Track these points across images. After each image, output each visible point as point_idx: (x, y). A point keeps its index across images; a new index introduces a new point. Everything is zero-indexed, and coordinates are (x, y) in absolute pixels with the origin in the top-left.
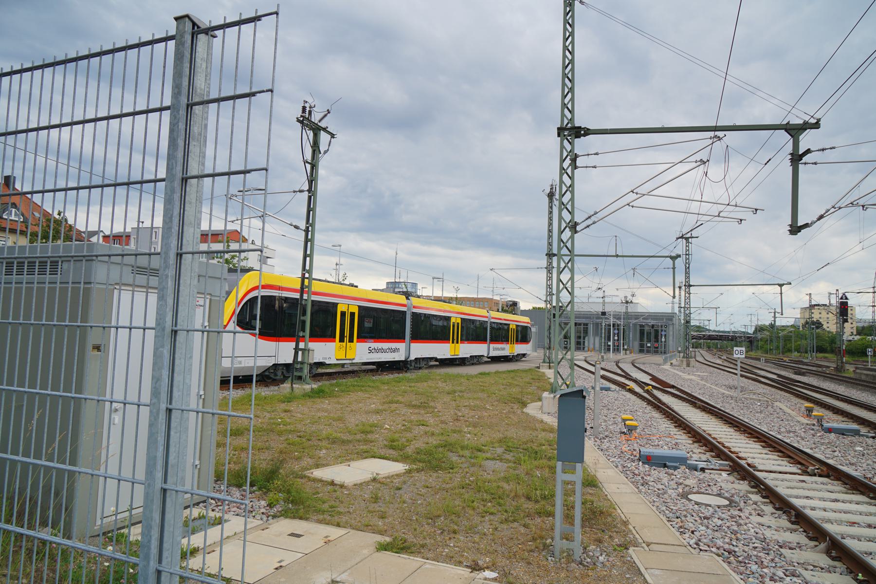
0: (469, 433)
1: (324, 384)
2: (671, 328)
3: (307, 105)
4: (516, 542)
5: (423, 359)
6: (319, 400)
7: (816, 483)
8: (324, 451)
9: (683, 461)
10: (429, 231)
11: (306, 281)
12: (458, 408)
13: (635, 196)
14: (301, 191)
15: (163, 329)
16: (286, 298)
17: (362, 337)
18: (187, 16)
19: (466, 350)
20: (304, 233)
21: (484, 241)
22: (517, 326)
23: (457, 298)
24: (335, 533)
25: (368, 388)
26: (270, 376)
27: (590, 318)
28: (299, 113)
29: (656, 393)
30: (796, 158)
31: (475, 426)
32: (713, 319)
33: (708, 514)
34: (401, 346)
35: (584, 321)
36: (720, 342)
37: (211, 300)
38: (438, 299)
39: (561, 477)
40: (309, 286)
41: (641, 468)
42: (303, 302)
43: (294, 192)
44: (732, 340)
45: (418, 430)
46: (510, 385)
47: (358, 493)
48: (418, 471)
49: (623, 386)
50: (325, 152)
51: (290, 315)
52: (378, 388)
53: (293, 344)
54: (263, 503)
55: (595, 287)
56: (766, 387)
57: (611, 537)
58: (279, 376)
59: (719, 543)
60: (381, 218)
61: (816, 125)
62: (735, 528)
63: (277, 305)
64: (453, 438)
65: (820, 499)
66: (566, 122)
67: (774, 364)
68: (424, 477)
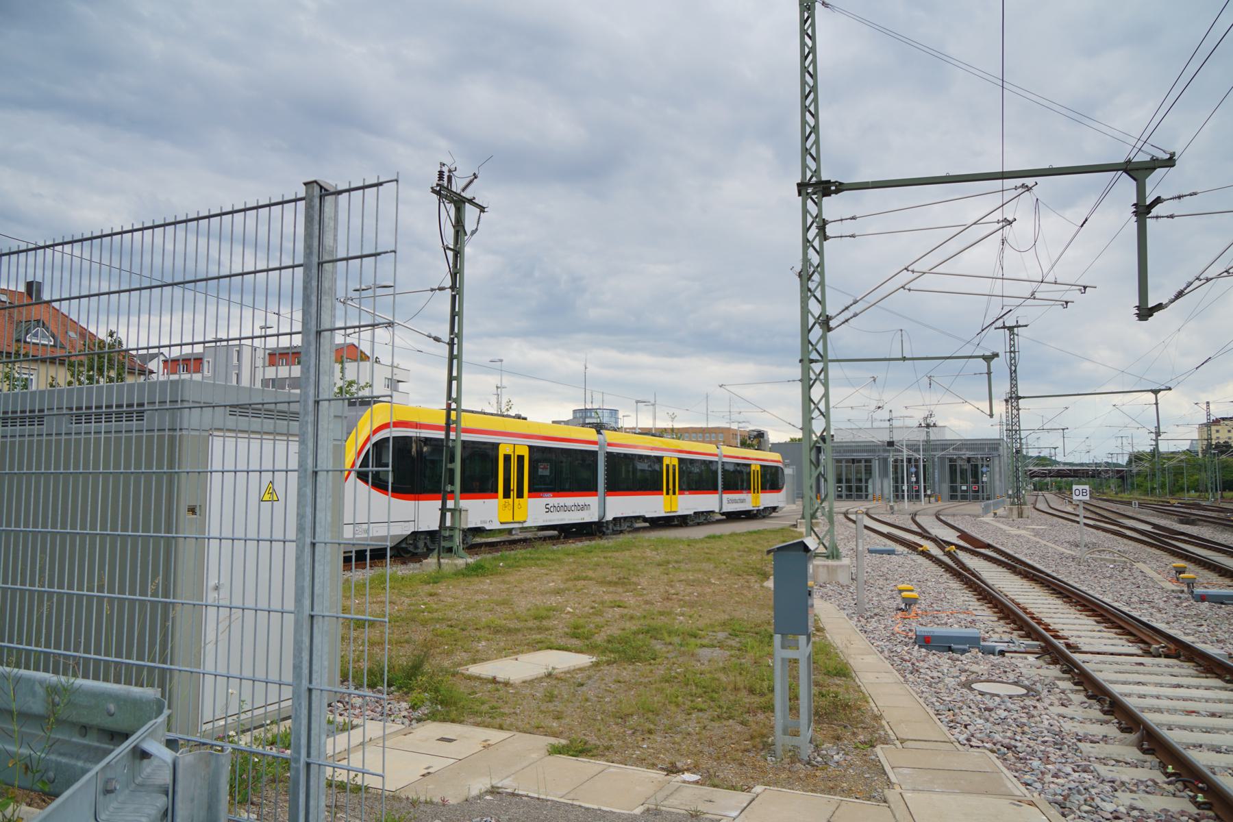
0: (683, 615)
1: (485, 557)
2: (997, 462)
3: (445, 169)
4: (729, 741)
5: (625, 518)
7: (1158, 665)
9: (974, 642)
10: (629, 331)
11: (453, 414)
12: (670, 584)
13: (910, 276)
14: (441, 289)
15: (306, 471)
17: (535, 490)
18: (315, 182)
19: (688, 503)
20: (447, 347)
21: (711, 342)
23: (673, 430)
24: (495, 736)
25: (545, 562)
26: (411, 549)
27: (874, 451)
28: (435, 180)
29: (964, 557)
30: (1143, 211)
31: (692, 605)
32: (1060, 444)
33: (991, 705)
34: (593, 501)
35: (865, 456)
36: (1056, 477)
38: (646, 432)
39: (781, 654)
40: (458, 421)
41: (915, 653)
42: (450, 444)
43: (432, 290)
44: (1093, 476)
45: (610, 614)
48: (609, 663)
49: (913, 547)
50: (473, 233)
51: (433, 462)
52: (558, 561)
53: (439, 503)
54: (404, 705)
55: (874, 405)
56: (1130, 542)
57: (854, 733)
58: (421, 548)
59: (998, 737)
60: (556, 316)
61: (1170, 162)
62: (1024, 720)
63: (414, 450)
64: (660, 621)
65: (1156, 685)
66: (809, 174)
67: (1154, 509)
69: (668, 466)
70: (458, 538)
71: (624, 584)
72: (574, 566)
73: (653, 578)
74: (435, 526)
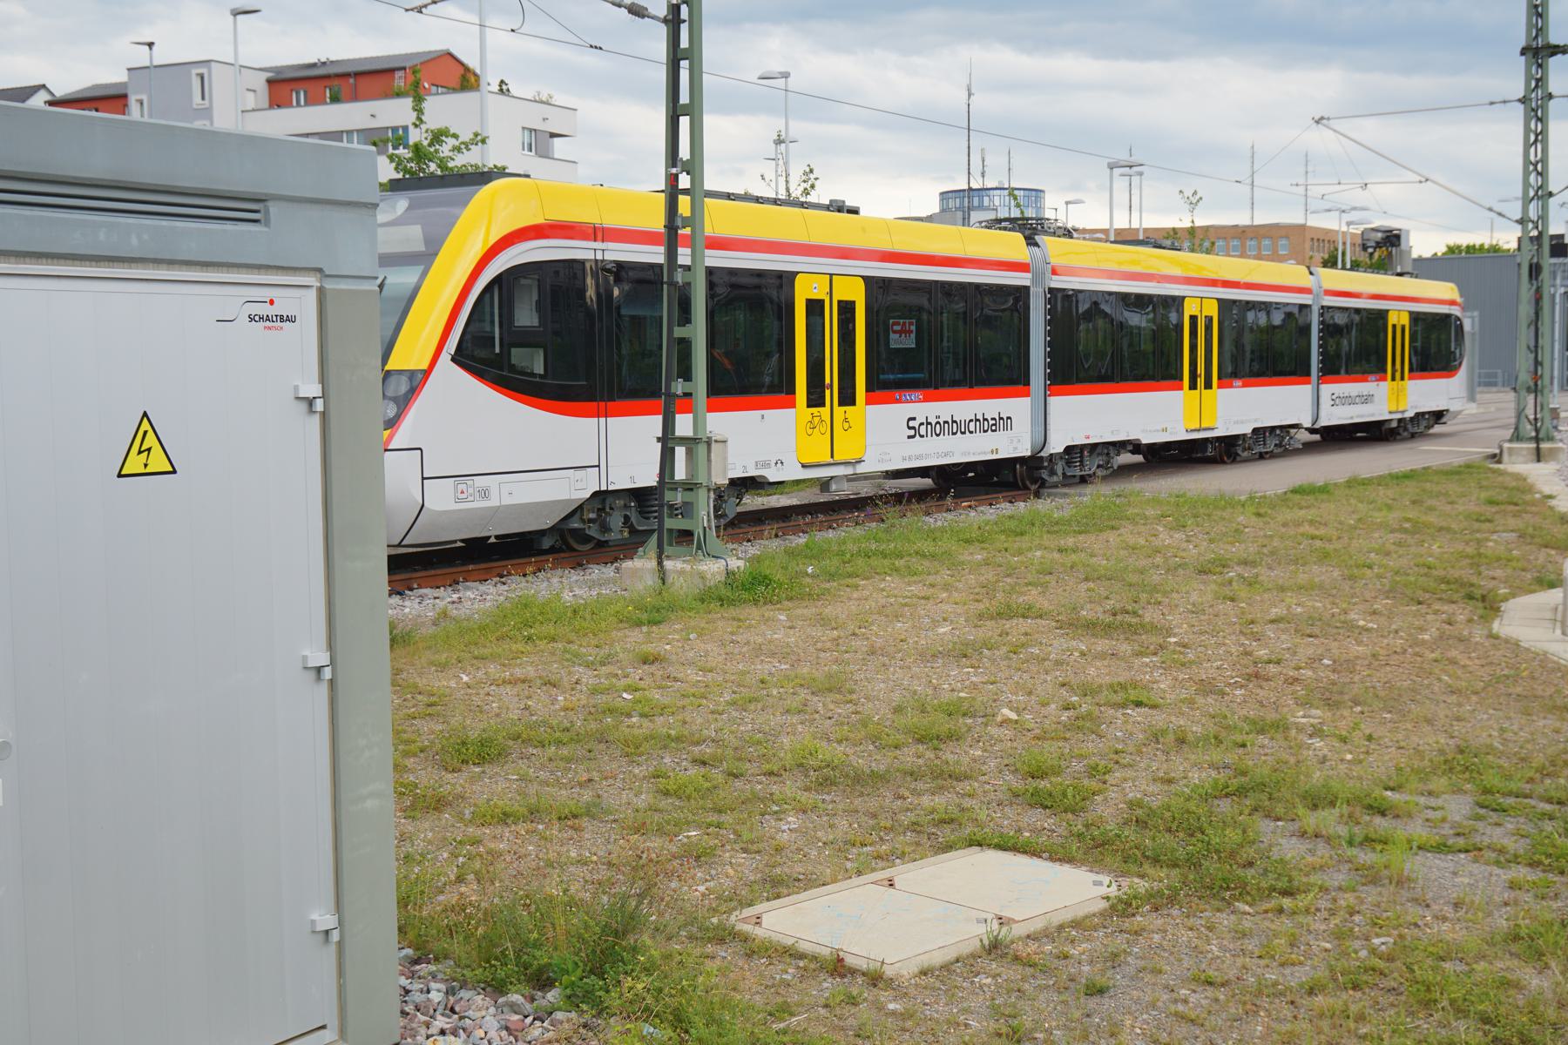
0: (1317, 732)
1: (768, 548)
6: (753, 613)
8: (793, 820)
11: (684, 203)
16: (620, 266)
17: (884, 385)
19: (1239, 408)
20: (662, 30)
22: (1224, 304)
23: (1192, 231)
34: (1017, 408)
37: (321, 292)
38: (1127, 238)
40: (695, 220)
45: (1127, 725)
46: (1417, 528)
47: (940, 1010)
48: (1159, 902)
51: (637, 322)
53: (655, 423)
58: (617, 529)
63: (591, 293)
64: (1264, 755)
68: (1185, 936)
69: (1193, 319)
70: (704, 507)
71: (1131, 631)
72: (989, 575)
73: (1196, 610)
74: (648, 477)
